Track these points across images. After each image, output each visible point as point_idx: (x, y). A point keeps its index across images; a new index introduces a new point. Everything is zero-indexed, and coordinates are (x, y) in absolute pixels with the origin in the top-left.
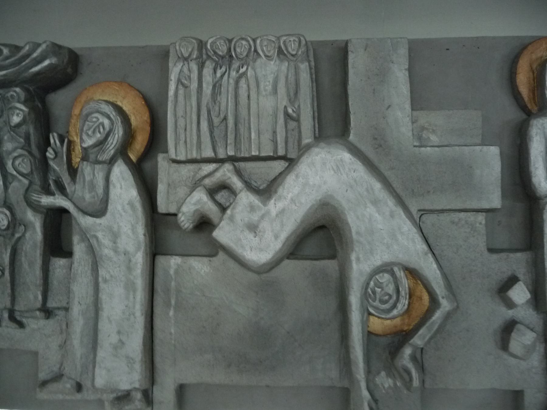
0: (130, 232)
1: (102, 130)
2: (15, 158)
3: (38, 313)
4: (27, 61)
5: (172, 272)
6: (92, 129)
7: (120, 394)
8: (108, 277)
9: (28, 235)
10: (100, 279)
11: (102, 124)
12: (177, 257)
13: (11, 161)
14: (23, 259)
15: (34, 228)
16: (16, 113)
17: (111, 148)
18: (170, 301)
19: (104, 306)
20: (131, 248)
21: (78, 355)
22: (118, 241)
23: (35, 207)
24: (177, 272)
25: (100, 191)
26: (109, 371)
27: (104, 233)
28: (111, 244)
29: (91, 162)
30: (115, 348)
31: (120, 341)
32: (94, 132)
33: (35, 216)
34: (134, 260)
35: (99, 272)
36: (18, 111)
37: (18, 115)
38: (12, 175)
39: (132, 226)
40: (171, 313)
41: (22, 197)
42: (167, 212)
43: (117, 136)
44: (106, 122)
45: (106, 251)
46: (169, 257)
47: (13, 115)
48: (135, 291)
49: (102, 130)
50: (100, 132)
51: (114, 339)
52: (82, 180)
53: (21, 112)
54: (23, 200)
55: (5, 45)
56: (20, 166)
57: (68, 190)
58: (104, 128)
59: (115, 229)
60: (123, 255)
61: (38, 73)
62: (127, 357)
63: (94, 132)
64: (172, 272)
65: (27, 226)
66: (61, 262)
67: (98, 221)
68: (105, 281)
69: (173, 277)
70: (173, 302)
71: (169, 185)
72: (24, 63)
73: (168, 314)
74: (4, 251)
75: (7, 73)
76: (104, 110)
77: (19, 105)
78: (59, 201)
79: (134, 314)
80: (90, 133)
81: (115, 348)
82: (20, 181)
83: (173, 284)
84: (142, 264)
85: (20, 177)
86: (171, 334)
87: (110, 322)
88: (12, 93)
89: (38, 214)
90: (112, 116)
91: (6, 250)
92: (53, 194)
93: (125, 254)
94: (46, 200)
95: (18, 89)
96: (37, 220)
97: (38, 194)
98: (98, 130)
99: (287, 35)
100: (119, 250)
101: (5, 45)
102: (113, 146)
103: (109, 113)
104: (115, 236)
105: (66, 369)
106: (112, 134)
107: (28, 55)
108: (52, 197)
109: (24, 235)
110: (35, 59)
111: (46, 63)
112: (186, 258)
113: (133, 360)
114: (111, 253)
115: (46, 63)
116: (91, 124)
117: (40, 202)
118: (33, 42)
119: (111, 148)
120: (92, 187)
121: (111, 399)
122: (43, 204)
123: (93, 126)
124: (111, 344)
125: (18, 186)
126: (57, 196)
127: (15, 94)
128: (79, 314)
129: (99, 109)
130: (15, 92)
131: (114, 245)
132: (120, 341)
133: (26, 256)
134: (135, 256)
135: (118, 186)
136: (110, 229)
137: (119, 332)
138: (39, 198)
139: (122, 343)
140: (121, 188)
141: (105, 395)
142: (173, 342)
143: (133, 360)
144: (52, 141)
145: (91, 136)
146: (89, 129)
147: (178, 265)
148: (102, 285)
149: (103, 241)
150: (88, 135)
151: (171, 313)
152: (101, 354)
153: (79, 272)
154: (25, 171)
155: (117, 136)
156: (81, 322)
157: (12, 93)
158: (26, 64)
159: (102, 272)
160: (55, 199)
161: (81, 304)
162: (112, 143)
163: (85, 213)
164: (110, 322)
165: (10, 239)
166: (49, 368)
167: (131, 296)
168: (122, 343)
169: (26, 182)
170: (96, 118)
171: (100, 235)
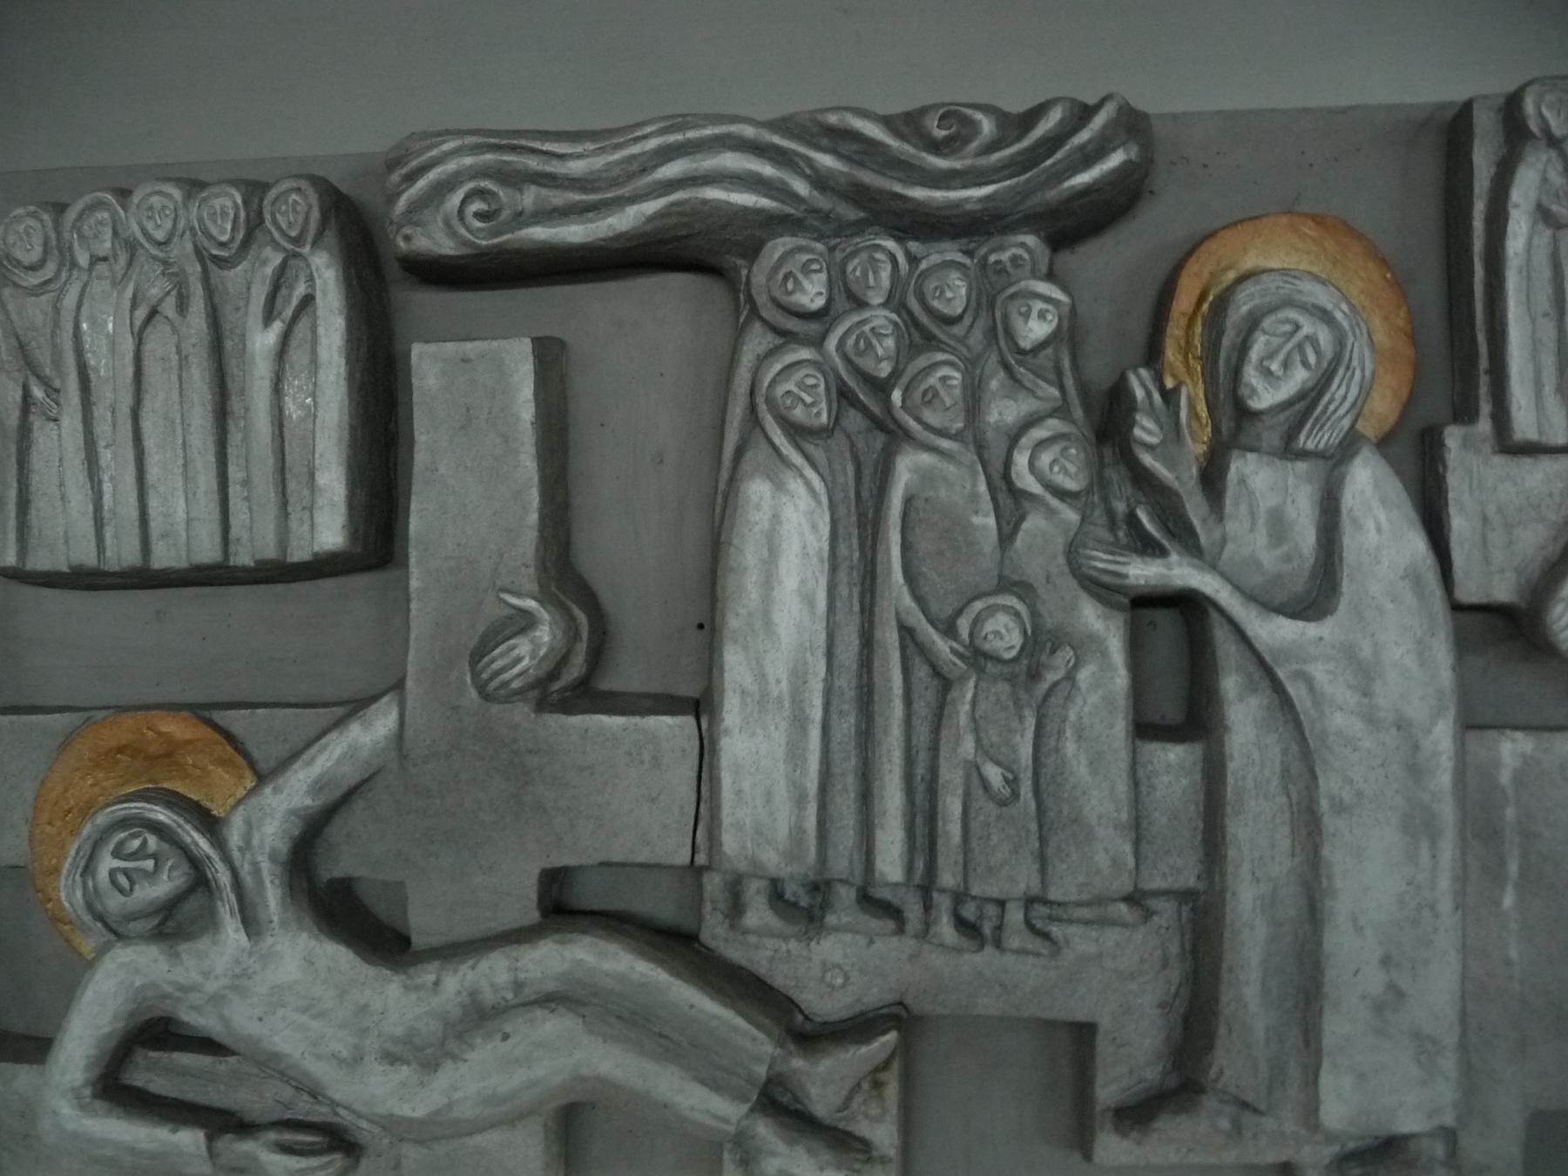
0: (1410, 662)
1: (1312, 359)
2: (1041, 444)
3: (1123, 908)
4: (1059, 155)
5: (1505, 777)
6: (1281, 356)
7: (1351, 1145)
8: (1347, 796)
9: (1084, 676)
10: (1324, 804)
11: (1313, 340)
12: (1519, 735)
13: (1027, 454)
14: (1070, 747)
15: (1104, 654)
16: (1034, 314)
17: (1341, 411)
18: (1502, 863)
19: (1339, 884)
20: (1417, 710)
21: (1260, 1033)
22: (1377, 687)
23: (1104, 590)
24: (1519, 778)
25: (1307, 537)
26: (1361, 1077)
27: (1331, 666)
28: (1352, 699)
29: (1268, 453)
30: (1379, 1008)
31: (1392, 987)
32: (1286, 365)
33: (1106, 618)
34: (1426, 744)
35: (1321, 782)
36: (1038, 305)
37: (1042, 315)
38: (1031, 496)
39: (1419, 642)
40: (1508, 900)
41: (1061, 560)
42: (1484, 600)
43: (1358, 374)
44: (1324, 336)
45: (1338, 720)
46: (1492, 734)
47: (1026, 316)
48: (1434, 837)
49: (1312, 359)
50: (1305, 364)
51: (1374, 981)
52: (1243, 509)
53: (1050, 307)
54: (1067, 570)
55: (986, 109)
56: (1056, 469)
57: (1203, 539)
58: (1318, 352)
59: (1366, 652)
60: (1394, 731)
61: (1086, 191)
62: (1417, 1036)
63: (1286, 365)
64: (1505, 777)
65: (1085, 646)
66: (1172, 756)
67: (1312, 630)
68: (1340, 808)
69: (1510, 792)
70: (1513, 868)
71: (1485, 520)
72: (1049, 162)
73: (1497, 903)
74: (1015, 724)
75: (996, 192)
76: (1312, 300)
77: (1043, 288)
78: (1179, 572)
79: (1432, 908)
80: (1275, 367)
81: (1379, 1008)
82: (1051, 512)
83: (1510, 813)
84: (1452, 754)
85: (1055, 502)
86: (1508, 963)
87: (1359, 929)
88: (1014, 251)
89: (1115, 613)
90: (1339, 316)
91: (1021, 718)
92: (1162, 552)
93: (1399, 728)
94: (1142, 572)
95: (1030, 240)
96: (1113, 629)
97: (1112, 553)
98: (1298, 358)
99: (847, 109)
100: (1382, 714)
101: (986, 109)
102: (1347, 404)
103: (1330, 307)
104: (1365, 675)
105: (1227, 1073)
106: (1341, 371)
107: (1053, 142)
108: (1159, 561)
109: (1070, 677)
110: (1082, 147)
111: (1115, 160)
112: (1546, 735)
113: (1434, 1042)
114: (1356, 726)
115: (1115, 160)
116: (1276, 341)
117: (1126, 576)
118: (1073, 101)
119: (1341, 411)
120: (1279, 527)
121: (1327, 1161)
122: (1132, 581)
123: (1281, 347)
124: (1364, 997)
125: (1044, 532)
126: (1174, 557)
127: (1026, 256)
128: (1254, 910)
129: (1297, 297)
130: (1023, 245)
131: (1365, 701)
132: (1392, 987)
133: (1079, 737)
134: (1430, 732)
135: (1370, 524)
136: (1349, 653)
137: (1386, 962)
138: (1118, 563)
139: (1397, 994)
140: (1379, 530)
141: (1307, 1150)
142: (1517, 987)
143: (1434, 1042)
144: (1139, 393)
145: (1278, 378)
146: (1271, 356)
147: (1523, 755)
148: (1330, 822)
149: (1329, 689)
150: (1268, 373)
151: (1508, 900)
152: (1335, 1028)
153: (1250, 783)
154: (1071, 485)
155: (1358, 374)
156: (1261, 931)
157: (1014, 251)
158: (1054, 164)
159: (1329, 784)
160: (1169, 567)
161: (1258, 881)
162: (1345, 398)
163: (1271, 607)
164: (1359, 929)
165: (1028, 690)
166: (1131, 1072)
167: (1425, 853)
168: (1397, 994)
169: (1071, 516)
170: (1288, 321)
171: (1319, 672)
